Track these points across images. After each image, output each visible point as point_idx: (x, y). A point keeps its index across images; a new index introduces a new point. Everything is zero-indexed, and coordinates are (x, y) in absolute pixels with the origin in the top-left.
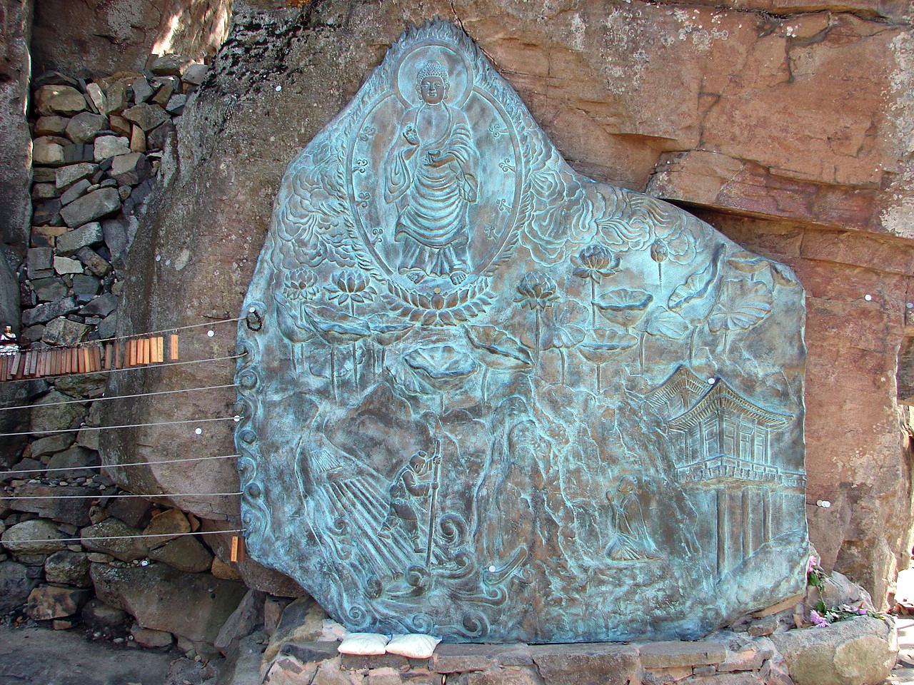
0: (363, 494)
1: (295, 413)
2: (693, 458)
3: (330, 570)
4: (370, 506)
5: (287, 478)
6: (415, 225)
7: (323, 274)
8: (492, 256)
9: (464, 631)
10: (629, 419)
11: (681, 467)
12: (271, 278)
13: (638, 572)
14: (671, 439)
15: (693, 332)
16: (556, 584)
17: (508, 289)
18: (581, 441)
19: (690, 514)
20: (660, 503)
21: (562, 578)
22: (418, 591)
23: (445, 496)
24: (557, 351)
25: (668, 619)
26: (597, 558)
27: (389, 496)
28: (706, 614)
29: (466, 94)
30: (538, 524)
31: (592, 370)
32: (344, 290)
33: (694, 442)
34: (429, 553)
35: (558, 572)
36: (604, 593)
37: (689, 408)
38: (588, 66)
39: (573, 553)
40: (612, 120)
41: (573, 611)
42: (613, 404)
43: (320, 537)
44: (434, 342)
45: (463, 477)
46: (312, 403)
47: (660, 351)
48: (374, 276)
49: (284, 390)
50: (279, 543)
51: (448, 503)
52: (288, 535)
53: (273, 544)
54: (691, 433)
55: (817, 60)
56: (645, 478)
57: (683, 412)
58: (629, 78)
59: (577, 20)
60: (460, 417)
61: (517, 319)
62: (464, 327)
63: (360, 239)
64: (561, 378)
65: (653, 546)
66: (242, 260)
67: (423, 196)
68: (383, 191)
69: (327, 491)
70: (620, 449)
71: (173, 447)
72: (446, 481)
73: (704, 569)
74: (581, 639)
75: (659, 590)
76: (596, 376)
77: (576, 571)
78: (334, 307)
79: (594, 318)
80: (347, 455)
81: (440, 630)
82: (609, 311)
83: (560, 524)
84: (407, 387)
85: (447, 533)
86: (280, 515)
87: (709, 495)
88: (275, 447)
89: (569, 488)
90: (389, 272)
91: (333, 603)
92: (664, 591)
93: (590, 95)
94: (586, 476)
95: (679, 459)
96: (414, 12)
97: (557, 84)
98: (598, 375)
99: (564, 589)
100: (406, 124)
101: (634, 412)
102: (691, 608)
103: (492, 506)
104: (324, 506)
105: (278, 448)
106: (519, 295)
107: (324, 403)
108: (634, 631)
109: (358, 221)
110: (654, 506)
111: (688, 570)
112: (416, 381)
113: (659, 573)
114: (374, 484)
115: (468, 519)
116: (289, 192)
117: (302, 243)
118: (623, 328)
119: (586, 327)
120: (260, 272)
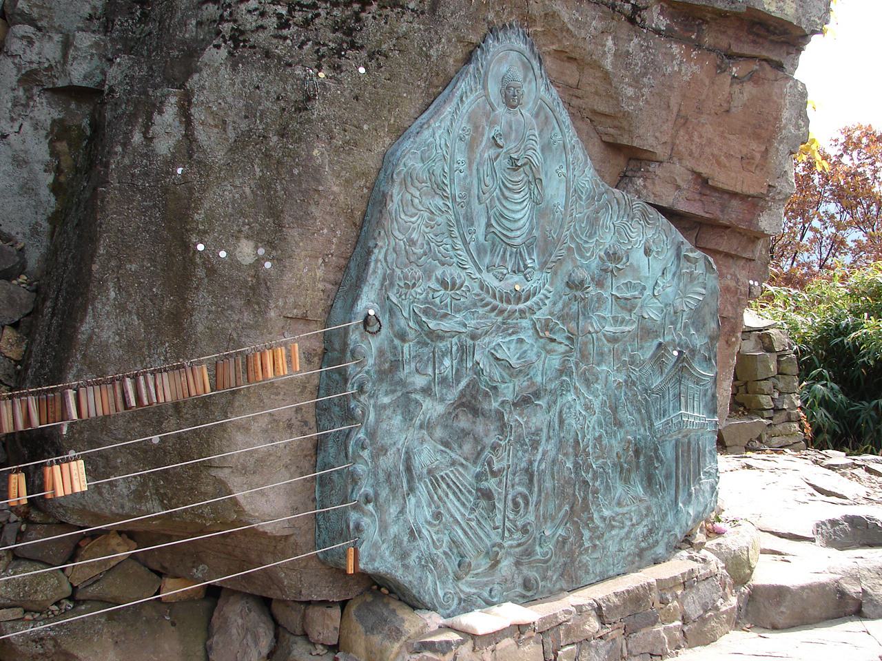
0: (454, 483)
1: (403, 414)
3: (426, 562)
4: (459, 494)
5: (393, 479)
6: (500, 225)
7: (428, 274)
8: (551, 255)
9: (524, 592)
12: (384, 279)
17: (560, 284)
18: (603, 413)
21: (590, 529)
22: (495, 564)
23: (514, 474)
24: (590, 336)
27: (474, 482)
29: (535, 103)
30: (577, 487)
31: (610, 351)
32: (446, 289)
33: (665, 403)
34: (504, 528)
35: (588, 525)
38: (611, 84)
40: (611, 131)
43: (420, 532)
44: (510, 335)
45: (527, 455)
46: (417, 402)
47: (646, 331)
48: (469, 275)
49: (393, 392)
50: (385, 546)
51: (517, 479)
52: (393, 536)
53: (380, 547)
55: (746, 96)
58: (637, 99)
59: (610, 43)
60: (524, 402)
61: (566, 310)
62: (532, 320)
63: (459, 238)
66: (327, 255)
67: (506, 198)
68: (476, 192)
69: (427, 486)
70: (624, 416)
71: (251, 463)
72: (516, 460)
74: (598, 578)
78: (436, 305)
80: (443, 449)
81: (507, 596)
84: (491, 379)
85: (516, 504)
86: (387, 518)
88: (383, 450)
90: (480, 271)
91: (430, 594)
93: (602, 108)
96: (497, 14)
97: (580, 95)
100: (493, 127)
101: (634, 383)
103: (548, 477)
104: (423, 501)
105: (387, 451)
106: (567, 290)
107: (427, 401)
109: (458, 221)
112: (497, 373)
114: (463, 472)
115: (531, 492)
116: (400, 190)
117: (412, 243)
120: (375, 272)
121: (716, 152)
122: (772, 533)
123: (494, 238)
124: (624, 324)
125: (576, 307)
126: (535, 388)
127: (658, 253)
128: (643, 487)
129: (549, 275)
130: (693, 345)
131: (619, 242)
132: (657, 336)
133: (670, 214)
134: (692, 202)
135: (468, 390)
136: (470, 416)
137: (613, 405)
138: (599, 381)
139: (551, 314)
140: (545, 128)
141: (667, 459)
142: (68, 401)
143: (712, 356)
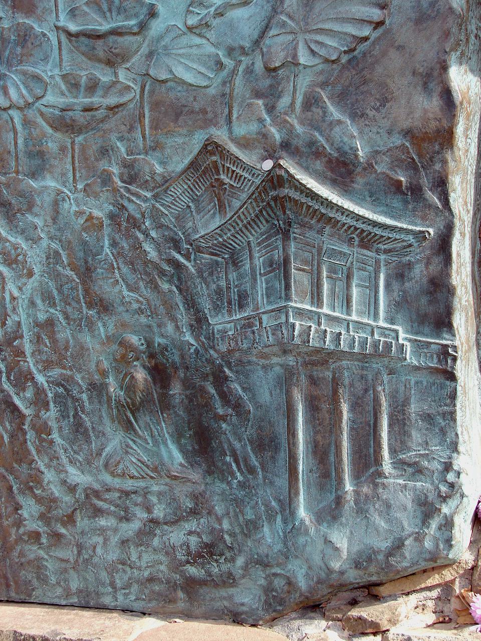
2: (241, 307)
10: (128, 236)
11: (219, 322)
13: (154, 499)
14: (200, 272)
15: (234, 72)
16: (29, 509)
19: (238, 406)
20: (187, 384)
21: (39, 500)
25: (208, 582)
26: (90, 472)
28: (271, 583)
31: (63, 149)
33: (241, 277)
36: (102, 531)
37: (229, 216)
39: (51, 460)
41: (61, 553)
42: (100, 208)
47: (172, 109)
54: (235, 262)
56: (158, 340)
57: (218, 224)
64: (13, 164)
65: (178, 457)
70: (115, 287)
73: (267, 505)
74: (75, 600)
75: (190, 533)
76: (69, 159)
77: (56, 491)
79: (60, 55)
82: (82, 39)
83: (27, 412)
87: (271, 375)
89: (40, 352)
92: (199, 535)
94: (64, 333)
95: (217, 308)
98: (73, 157)
99: (42, 517)
101: (135, 223)
102: (246, 568)
108: (100, 395)
110: (176, 389)
111: (238, 503)
113: (190, 504)
118: (108, 70)
119: (49, 71)
122: (411, 575)
124: (100, 92)
128: (182, 450)
138: (36, 209)
141: (258, 406)
142: (298, 415)
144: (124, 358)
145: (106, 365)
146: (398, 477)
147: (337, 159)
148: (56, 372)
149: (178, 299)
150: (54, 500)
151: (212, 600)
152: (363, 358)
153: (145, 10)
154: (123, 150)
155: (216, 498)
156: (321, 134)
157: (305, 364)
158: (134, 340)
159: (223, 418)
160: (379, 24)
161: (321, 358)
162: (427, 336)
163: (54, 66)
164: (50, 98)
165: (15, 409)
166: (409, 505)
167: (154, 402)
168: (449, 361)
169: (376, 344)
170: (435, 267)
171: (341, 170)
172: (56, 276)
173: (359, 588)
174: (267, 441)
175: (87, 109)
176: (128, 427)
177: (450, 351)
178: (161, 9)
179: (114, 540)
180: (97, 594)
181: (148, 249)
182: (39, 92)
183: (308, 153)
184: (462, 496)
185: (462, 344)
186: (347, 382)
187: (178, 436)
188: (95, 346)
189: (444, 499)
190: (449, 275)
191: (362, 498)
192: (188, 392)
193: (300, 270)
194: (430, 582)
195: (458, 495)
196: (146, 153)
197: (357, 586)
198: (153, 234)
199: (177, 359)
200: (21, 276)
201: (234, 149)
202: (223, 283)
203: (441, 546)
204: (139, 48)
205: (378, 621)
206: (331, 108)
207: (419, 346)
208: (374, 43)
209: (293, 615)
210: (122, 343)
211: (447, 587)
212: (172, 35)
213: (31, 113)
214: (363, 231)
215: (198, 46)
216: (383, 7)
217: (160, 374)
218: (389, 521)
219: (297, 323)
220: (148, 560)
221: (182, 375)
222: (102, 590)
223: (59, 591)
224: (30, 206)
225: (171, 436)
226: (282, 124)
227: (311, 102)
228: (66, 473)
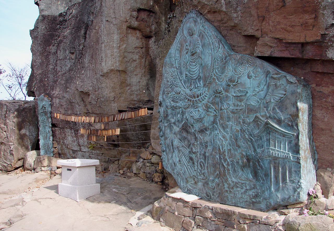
8: (207, 82)
10: (243, 133)
11: (259, 150)
14: (255, 141)
15: (261, 103)
16: (226, 186)
17: (211, 92)
19: (261, 167)
20: (253, 162)
21: (228, 184)
23: (200, 155)
28: (267, 203)
31: (233, 117)
33: (262, 142)
36: (238, 191)
41: (231, 195)
42: (239, 128)
44: (196, 108)
47: (251, 110)
49: (167, 122)
51: (201, 157)
54: (261, 139)
56: (248, 153)
60: (202, 131)
61: (214, 101)
63: (179, 79)
70: (241, 143)
75: (253, 192)
80: (180, 141)
82: (236, 97)
83: (226, 166)
87: (267, 161)
92: (254, 193)
94: (232, 152)
95: (258, 148)
96: (187, 9)
99: (228, 187)
102: (262, 200)
105: (167, 139)
108: (238, 164)
110: (251, 163)
117: (168, 81)
118: (240, 103)
119: (231, 103)
121: (283, 26)
123: (188, 78)
124: (239, 107)
125: (217, 100)
126: (205, 127)
127: (255, 77)
128: (252, 176)
129: (207, 89)
130: (278, 118)
131: (235, 74)
132: (257, 112)
133: (270, 60)
134: (283, 52)
135: (184, 125)
136: (186, 133)
137: (235, 138)
138: (228, 128)
139: (208, 102)
140: (202, 39)
143: (294, 124)
144: (242, 156)
145: (239, 158)
146: (289, 183)
147: (278, 120)
148: (231, 159)
149: (251, 146)
150: (230, 184)
151: (257, 206)
152: (283, 159)
153: (246, 92)
154: (242, 117)
155: (258, 185)
156: (276, 115)
157: (273, 159)
158: (244, 153)
159: (259, 169)
160: (285, 95)
161: (276, 158)
162: (295, 155)
163: (231, 102)
164: (231, 108)
165: (224, 166)
166: (292, 189)
167: (247, 166)
168: (299, 160)
169: (285, 156)
170: (296, 141)
171: (279, 122)
172: (231, 141)
173: (285, 206)
174: (267, 174)
175: (236, 110)
176: (243, 170)
177: (299, 158)
178: (249, 91)
179: (240, 193)
180: (237, 204)
181: (246, 136)
182: (229, 106)
183: (273, 118)
184: (302, 188)
185: (302, 157)
186: (281, 163)
187: (251, 173)
188: (238, 154)
189: (298, 188)
190: (299, 143)
191: (283, 187)
192: (253, 164)
193: (272, 141)
194: (298, 206)
195: (301, 187)
196: (246, 118)
197: (283, 206)
198: (247, 133)
199: (251, 158)
200: (226, 140)
201: (261, 117)
202: (259, 143)
203: (298, 198)
204: (245, 99)
205: (285, 212)
206: (277, 110)
207: (293, 157)
208: (284, 98)
209: (271, 210)
210: (242, 154)
211: (302, 207)
212: (251, 96)
213: (228, 110)
214: (283, 134)
215: (255, 98)
216: (285, 91)
217: (248, 160)
218: (288, 192)
219: (271, 151)
220: (246, 197)
221: (252, 161)
222: (238, 203)
223: (231, 203)
224: (227, 127)
225: (250, 173)
226: (269, 113)
227: (274, 109)
228: (232, 179)
